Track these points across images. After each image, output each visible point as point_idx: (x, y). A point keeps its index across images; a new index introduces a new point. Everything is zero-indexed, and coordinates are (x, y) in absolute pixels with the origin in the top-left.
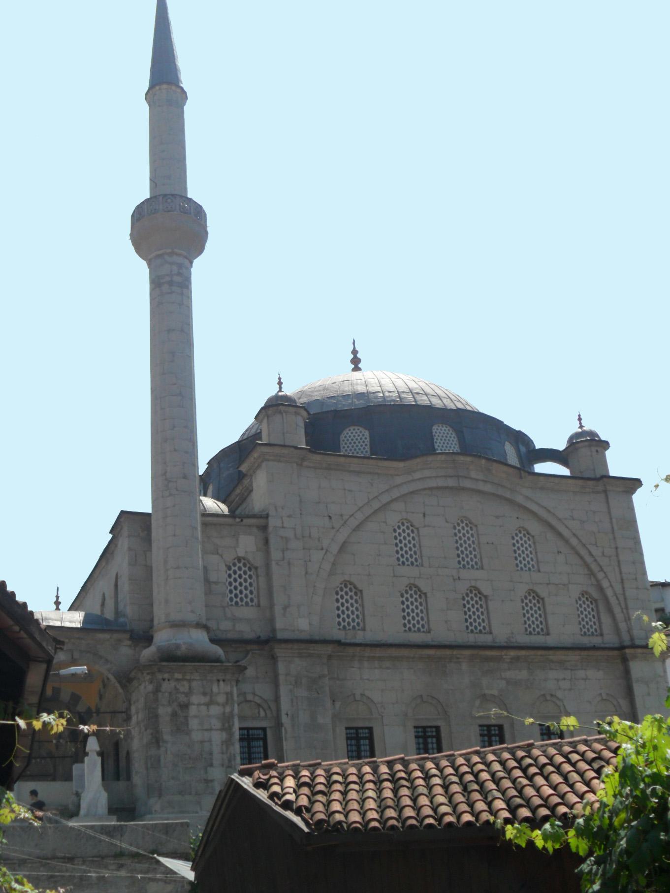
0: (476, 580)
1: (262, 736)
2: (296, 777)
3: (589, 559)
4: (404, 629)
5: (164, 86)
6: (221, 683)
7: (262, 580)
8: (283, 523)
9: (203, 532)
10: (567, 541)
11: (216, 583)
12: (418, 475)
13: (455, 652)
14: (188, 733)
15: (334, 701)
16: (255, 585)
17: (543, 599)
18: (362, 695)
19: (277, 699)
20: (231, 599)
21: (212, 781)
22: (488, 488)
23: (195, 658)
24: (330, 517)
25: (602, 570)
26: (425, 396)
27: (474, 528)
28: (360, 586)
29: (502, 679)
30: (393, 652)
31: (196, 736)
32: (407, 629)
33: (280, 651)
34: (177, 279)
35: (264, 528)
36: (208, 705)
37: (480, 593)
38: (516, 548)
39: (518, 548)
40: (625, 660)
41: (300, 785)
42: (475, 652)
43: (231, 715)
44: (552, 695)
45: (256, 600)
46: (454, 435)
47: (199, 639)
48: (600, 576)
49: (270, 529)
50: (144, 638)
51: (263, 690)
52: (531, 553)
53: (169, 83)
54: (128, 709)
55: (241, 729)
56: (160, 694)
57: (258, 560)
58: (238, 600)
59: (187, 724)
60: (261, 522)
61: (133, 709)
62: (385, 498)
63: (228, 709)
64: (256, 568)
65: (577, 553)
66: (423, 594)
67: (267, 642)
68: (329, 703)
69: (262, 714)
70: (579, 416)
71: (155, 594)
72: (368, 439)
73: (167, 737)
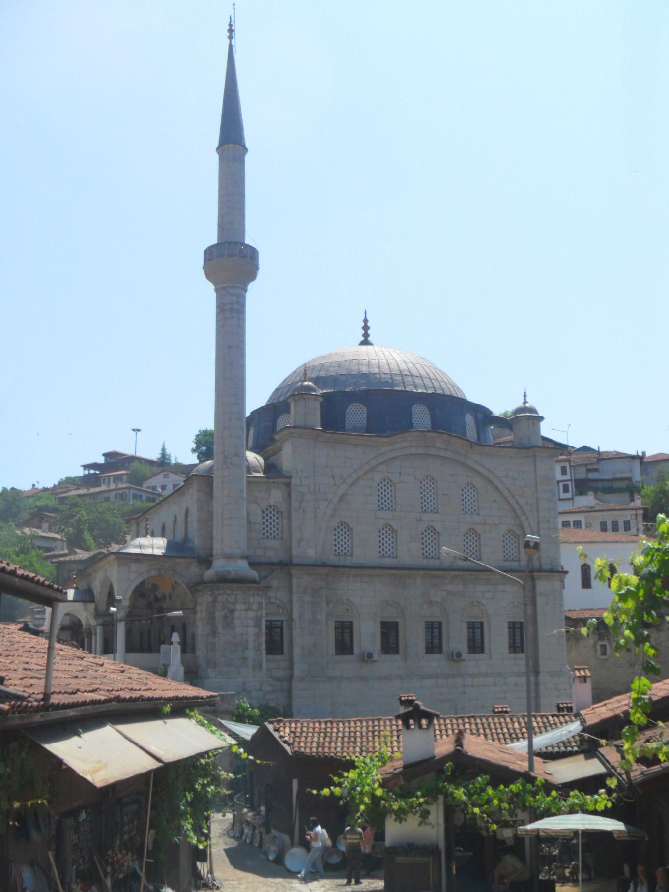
0: (432, 521)
1: (279, 626)
2: (290, 728)
3: (516, 507)
4: (379, 555)
5: (231, 145)
6: (256, 596)
7: (285, 521)
8: (301, 482)
9: (247, 488)
10: (501, 493)
12: (397, 446)
13: (413, 572)
15: (328, 604)
16: (280, 524)
17: (479, 534)
18: (348, 600)
19: (291, 602)
20: (264, 534)
22: (448, 454)
23: (240, 581)
24: (333, 477)
25: (524, 514)
26: (410, 377)
27: (435, 483)
28: (351, 526)
30: (371, 572)
31: (239, 630)
32: (381, 555)
33: (295, 572)
34: (235, 307)
35: (288, 485)
36: (246, 610)
37: (435, 530)
38: (464, 498)
39: (466, 498)
40: (533, 579)
42: (427, 572)
43: (261, 617)
44: (478, 602)
45: (280, 535)
46: (428, 412)
47: (242, 567)
48: (523, 518)
49: (292, 486)
50: (206, 561)
51: (282, 596)
52: (474, 501)
53: (235, 143)
55: (266, 621)
56: (217, 604)
58: (269, 534)
59: (233, 623)
60: (287, 481)
61: (198, 608)
62: (373, 463)
63: (259, 613)
64: (282, 513)
65: (508, 501)
66: (394, 531)
67: (286, 565)
69: (281, 611)
70: (525, 393)
71: (215, 533)
72: (366, 414)
73: (220, 630)
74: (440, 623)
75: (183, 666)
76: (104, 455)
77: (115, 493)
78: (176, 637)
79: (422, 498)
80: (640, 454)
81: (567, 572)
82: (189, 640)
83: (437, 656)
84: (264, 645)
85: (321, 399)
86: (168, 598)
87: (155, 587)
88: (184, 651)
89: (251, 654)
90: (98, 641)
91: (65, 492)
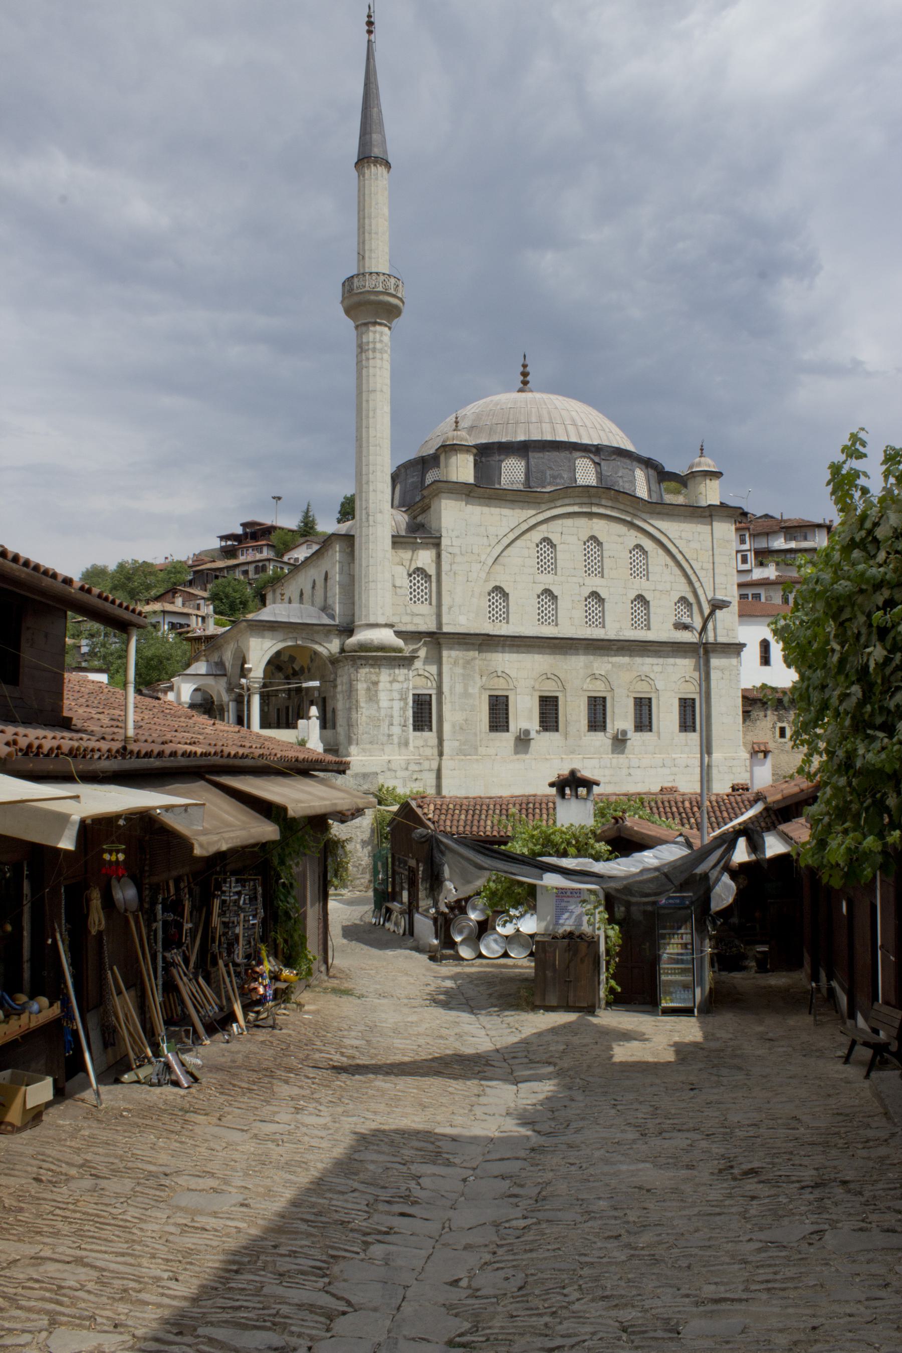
11: (400, 587)
12: (298, 1242)
14: (377, 702)
21: (392, 735)
29: (609, 663)
36: (391, 682)
41: (435, 809)
49: (443, 547)
54: (335, 680)
55: (414, 695)
57: (432, 571)
61: (339, 681)
63: (405, 686)
68: (477, 677)
74: (604, 698)
75: (322, 742)
76: (242, 525)
77: (254, 565)
78: (314, 711)
79: (585, 561)
80: (828, 522)
81: (744, 645)
82: (329, 715)
83: (600, 735)
84: (411, 721)
85: (475, 451)
86: (306, 670)
87: (292, 659)
88: (324, 726)
89: (396, 730)
90: (231, 714)
91: (199, 565)
